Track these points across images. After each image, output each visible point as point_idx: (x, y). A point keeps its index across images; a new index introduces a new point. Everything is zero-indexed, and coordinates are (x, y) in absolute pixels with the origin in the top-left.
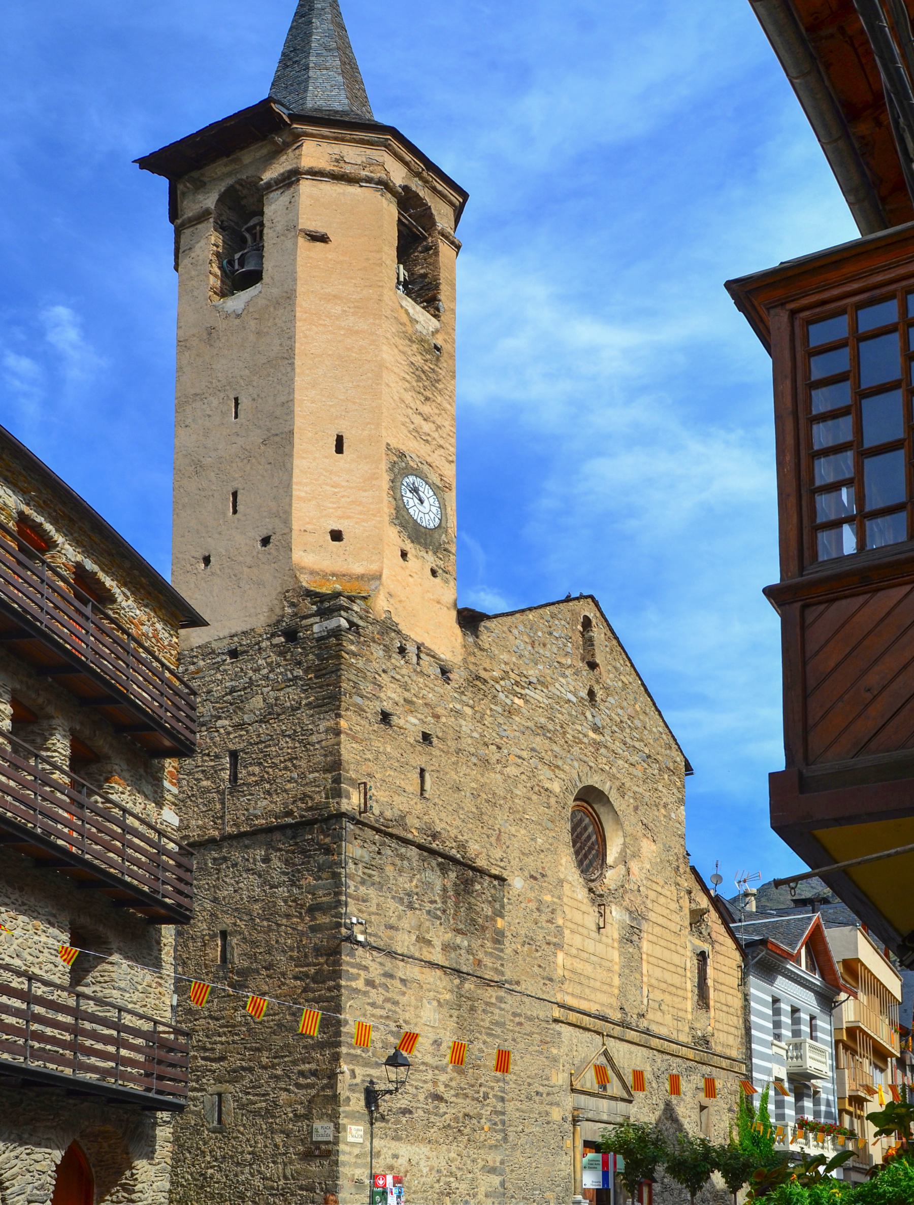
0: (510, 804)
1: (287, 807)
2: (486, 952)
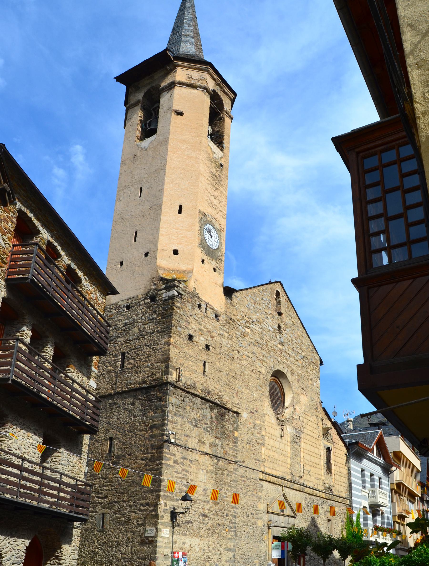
0: (242, 378)
1: (144, 379)
2: (229, 447)
